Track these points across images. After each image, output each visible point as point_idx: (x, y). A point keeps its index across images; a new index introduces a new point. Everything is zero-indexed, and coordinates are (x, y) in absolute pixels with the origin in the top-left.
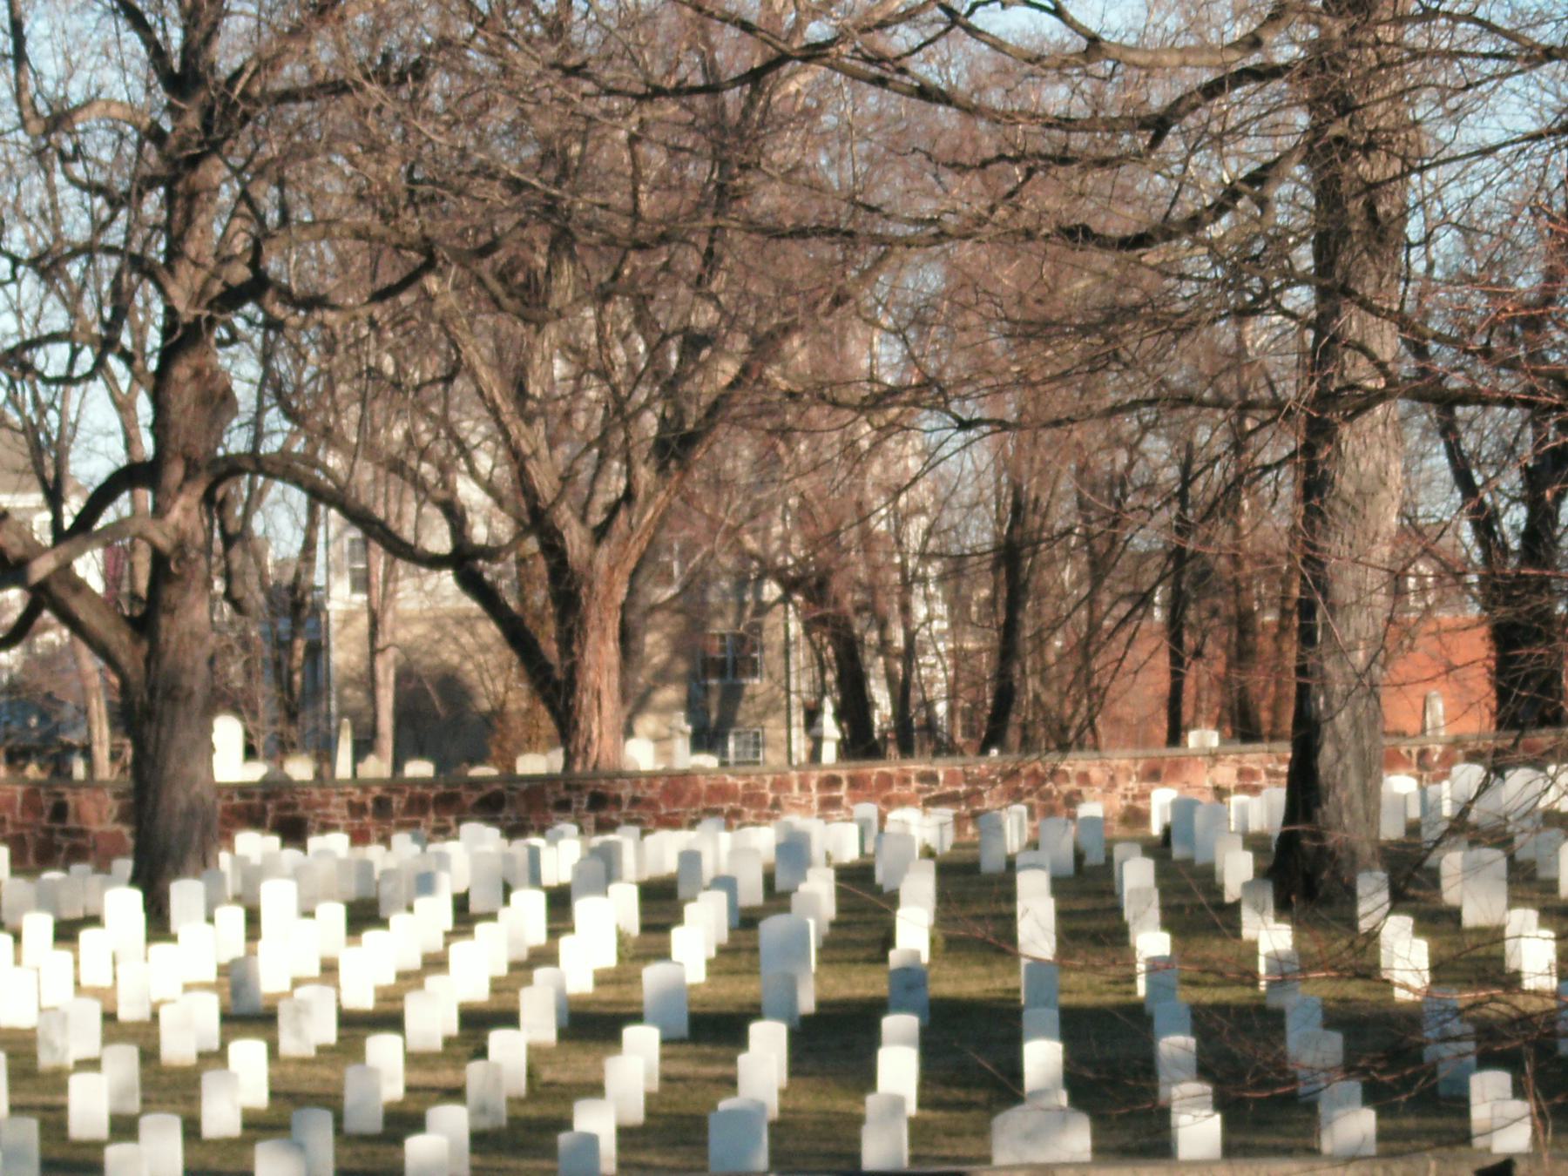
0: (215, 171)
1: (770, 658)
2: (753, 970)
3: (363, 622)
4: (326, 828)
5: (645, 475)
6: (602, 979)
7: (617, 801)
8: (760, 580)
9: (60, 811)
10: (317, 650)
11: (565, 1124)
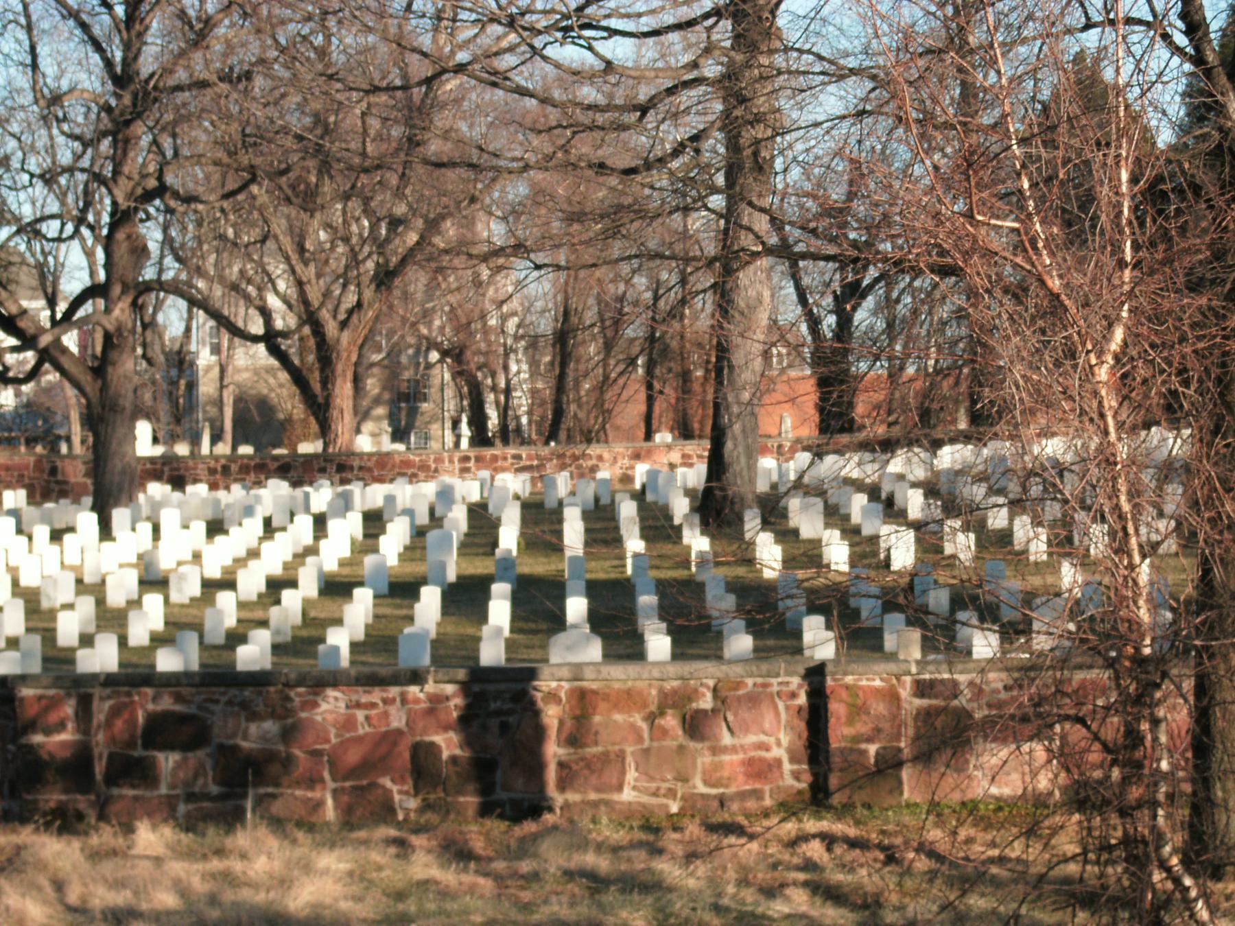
0: (139, 128)
1: (433, 392)
2: (423, 559)
4: (196, 481)
5: (368, 294)
6: (342, 563)
7: (352, 468)
8: (428, 350)
9: (54, 471)
10: (192, 386)
11: (322, 640)
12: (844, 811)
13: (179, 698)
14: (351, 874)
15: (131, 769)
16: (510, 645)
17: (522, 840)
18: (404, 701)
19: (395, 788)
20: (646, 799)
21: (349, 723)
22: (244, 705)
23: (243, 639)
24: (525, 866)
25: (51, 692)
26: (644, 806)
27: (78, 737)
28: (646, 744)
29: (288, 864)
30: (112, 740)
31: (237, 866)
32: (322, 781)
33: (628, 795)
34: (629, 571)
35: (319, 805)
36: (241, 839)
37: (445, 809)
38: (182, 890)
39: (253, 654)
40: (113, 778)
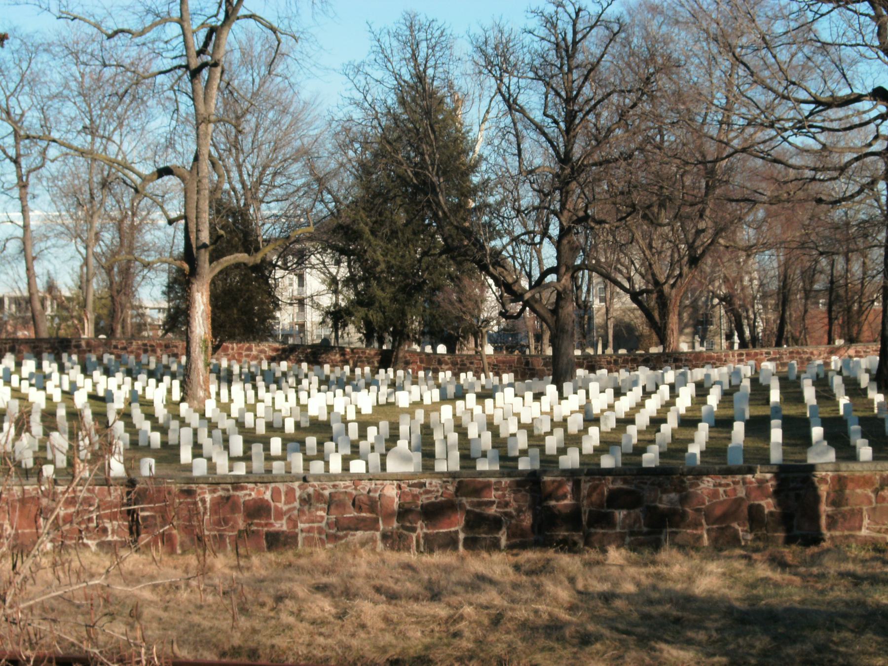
0: (574, 185)
1: (715, 320)
2: (732, 407)
3: (604, 310)
4: (600, 368)
5: (686, 269)
6: (688, 410)
7: (681, 360)
8: (712, 298)
9: (527, 363)
10: (591, 318)
11: (686, 450)
13: (625, 482)
14: (724, 574)
15: (602, 519)
16: (784, 453)
17: (812, 556)
18: (744, 483)
19: (740, 529)
20: (874, 534)
21: (715, 494)
22: (660, 485)
23: (644, 450)
24: (815, 570)
25: (559, 479)
26: (873, 538)
27: (573, 502)
28: (874, 505)
30: (592, 504)
31: (664, 570)
32: (701, 524)
33: (864, 532)
34: (842, 412)
35: (699, 538)
36: (663, 555)
37: (767, 540)
38: (638, 584)
40: (591, 524)
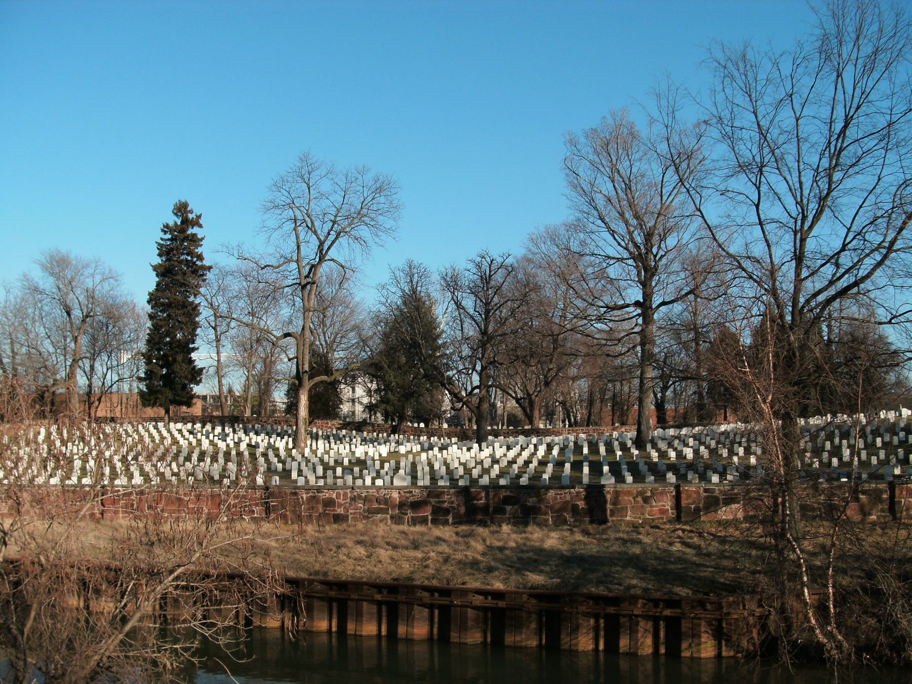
0: (488, 345)
10: (496, 411)
12: (686, 523)
15: (499, 510)
21: (556, 499)
24: (604, 537)
29: (543, 535)
30: (494, 503)
31: (530, 536)
33: (628, 518)
35: (548, 520)
36: (530, 529)
37: (581, 521)
39: (524, 481)
